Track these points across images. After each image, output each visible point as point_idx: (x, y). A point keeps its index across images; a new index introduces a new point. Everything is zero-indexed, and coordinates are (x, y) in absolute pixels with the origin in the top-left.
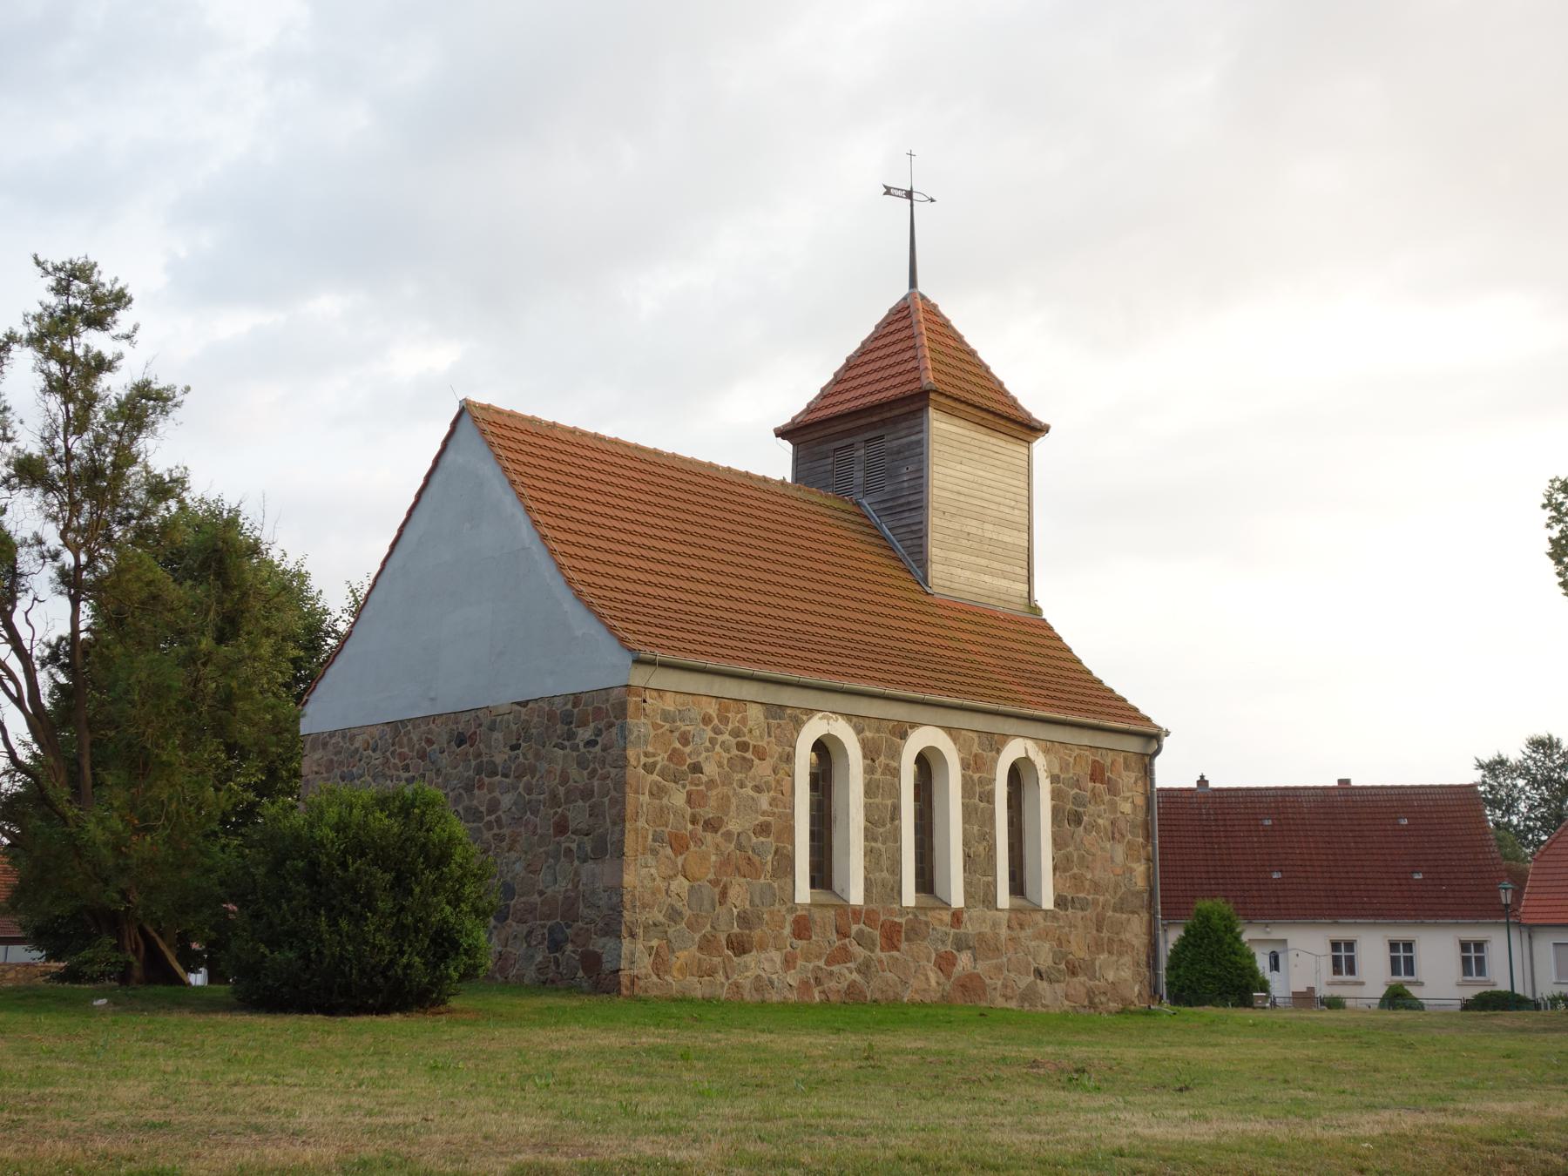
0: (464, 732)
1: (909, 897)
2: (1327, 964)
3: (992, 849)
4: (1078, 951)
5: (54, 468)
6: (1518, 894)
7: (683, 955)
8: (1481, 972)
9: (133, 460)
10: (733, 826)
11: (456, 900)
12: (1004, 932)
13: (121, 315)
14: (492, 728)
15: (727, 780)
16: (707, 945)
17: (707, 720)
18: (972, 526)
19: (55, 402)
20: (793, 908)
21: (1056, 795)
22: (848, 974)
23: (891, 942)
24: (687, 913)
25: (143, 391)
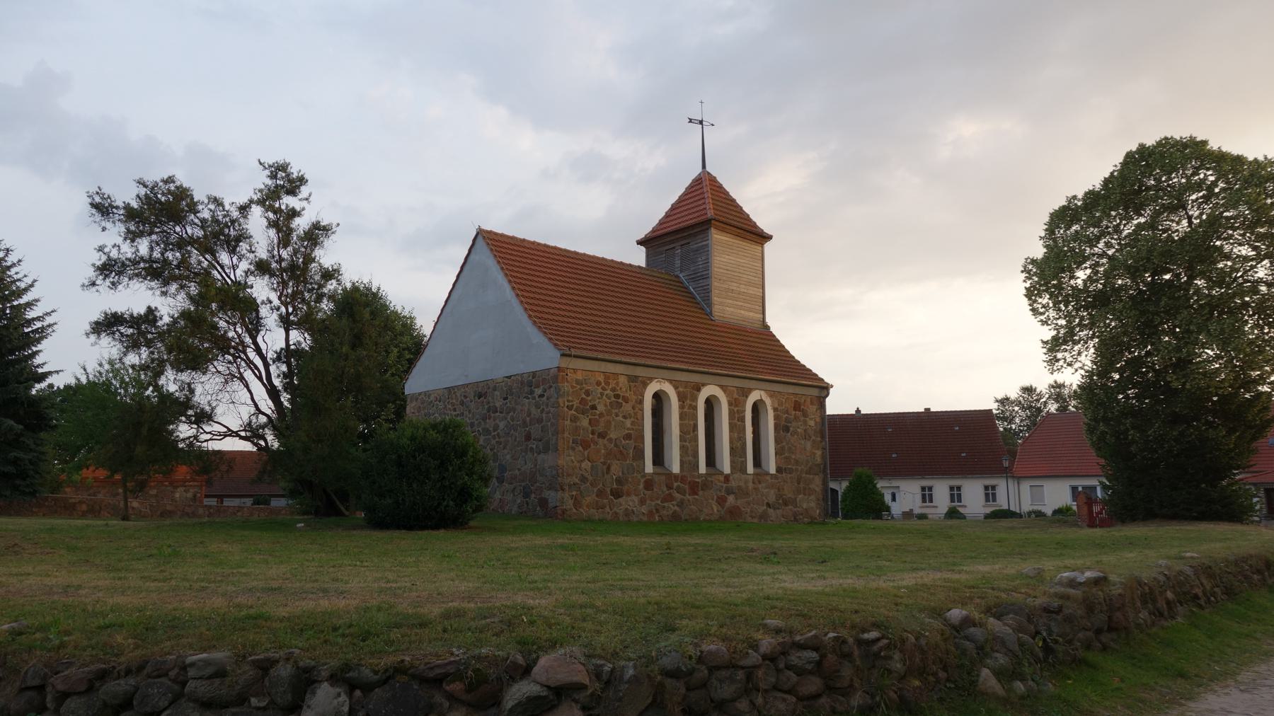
0: (482, 391)
1: (703, 468)
2: (919, 497)
3: (744, 444)
4: (788, 493)
5: (274, 265)
6: (1012, 463)
7: (589, 499)
8: (994, 500)
9: (313, 260)
10: (613, 435)
11: (470, 474)
12: (751, 485)
13: (303, 188)
14: (495, 389)
15: (609, 413)
16: (600, 494)
17: (598, 383)
18: (734, 286)
19: (272, 232)
20: (645, 475)
21: (776, 418)
22: (672, 507)
23: (694, 491)
24: (590, 478)
25: (316, 226)
